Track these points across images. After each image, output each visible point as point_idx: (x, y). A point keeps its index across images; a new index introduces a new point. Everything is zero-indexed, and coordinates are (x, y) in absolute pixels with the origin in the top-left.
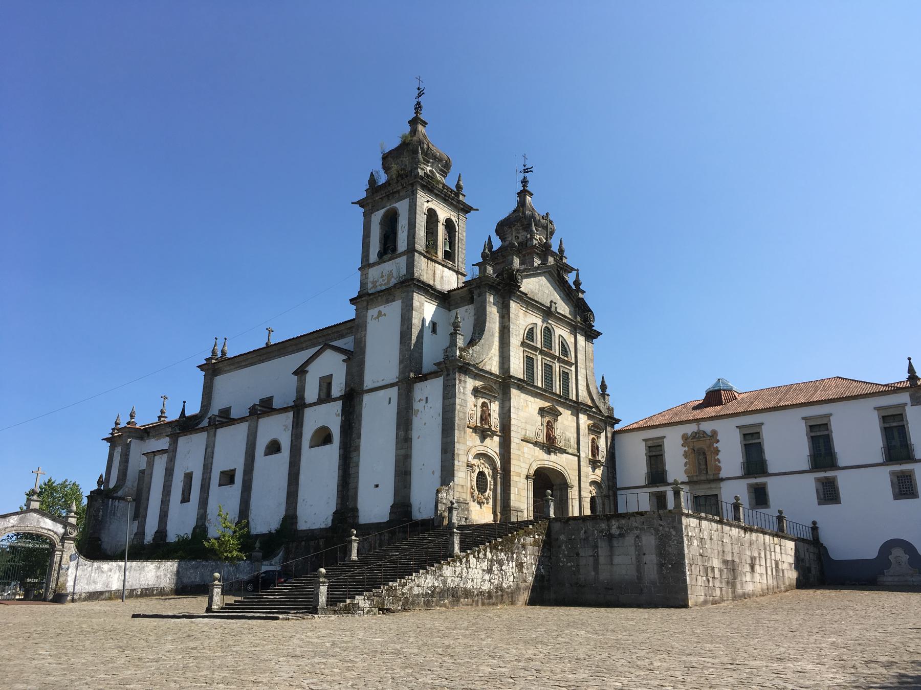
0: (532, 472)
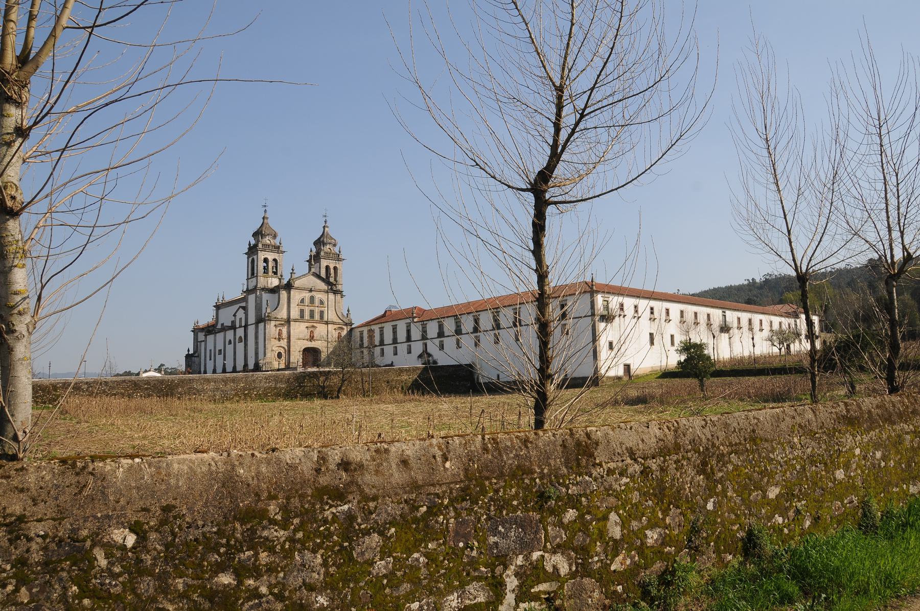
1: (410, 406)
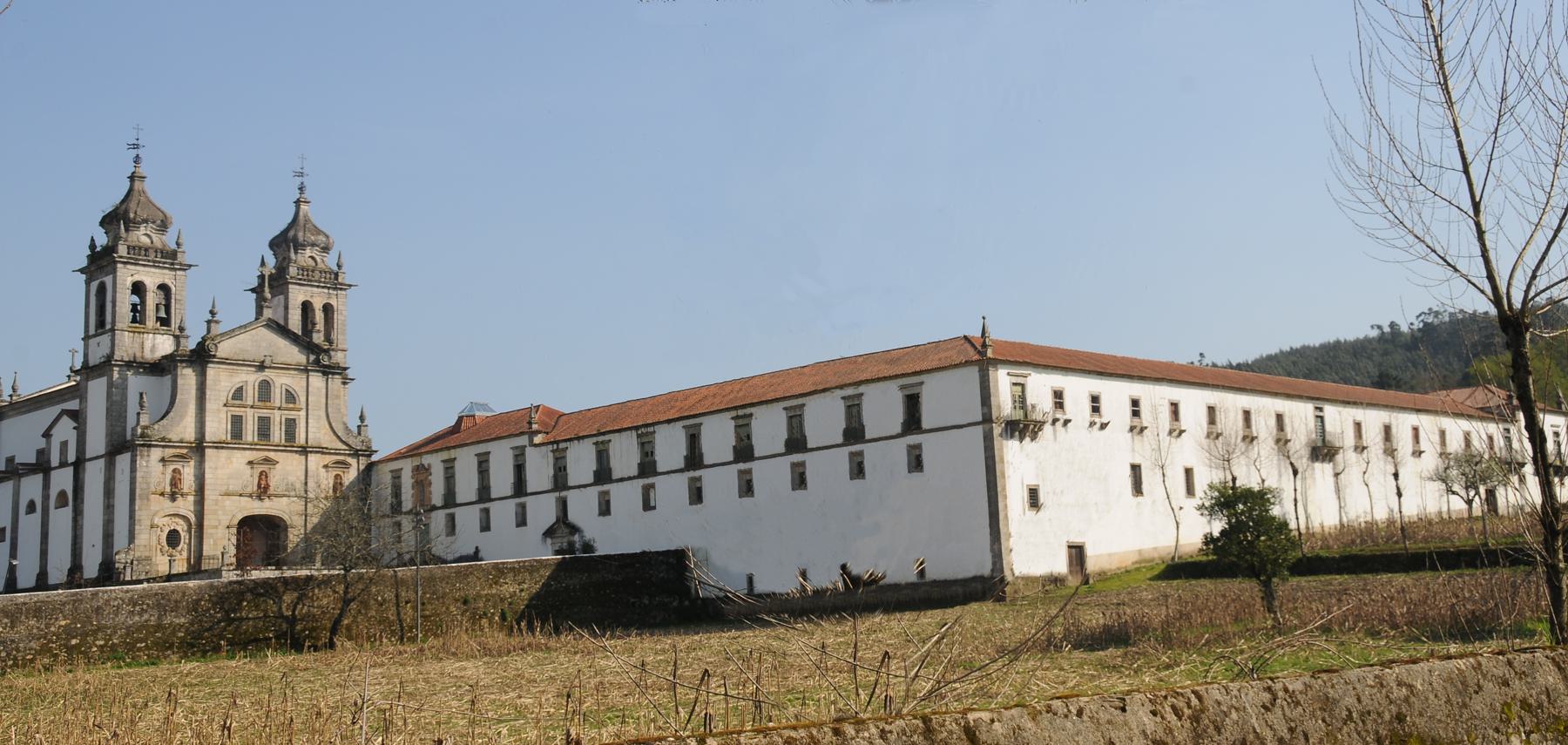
0: (236, 522)
1: (523, 663)
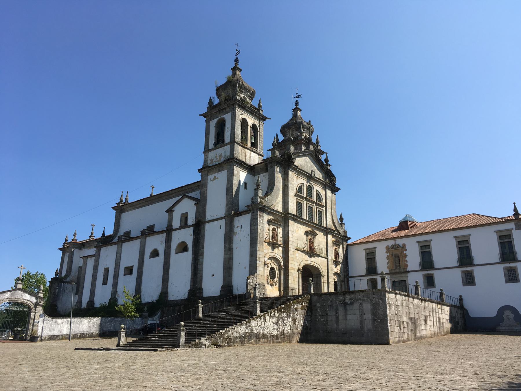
0: (301, 267)
